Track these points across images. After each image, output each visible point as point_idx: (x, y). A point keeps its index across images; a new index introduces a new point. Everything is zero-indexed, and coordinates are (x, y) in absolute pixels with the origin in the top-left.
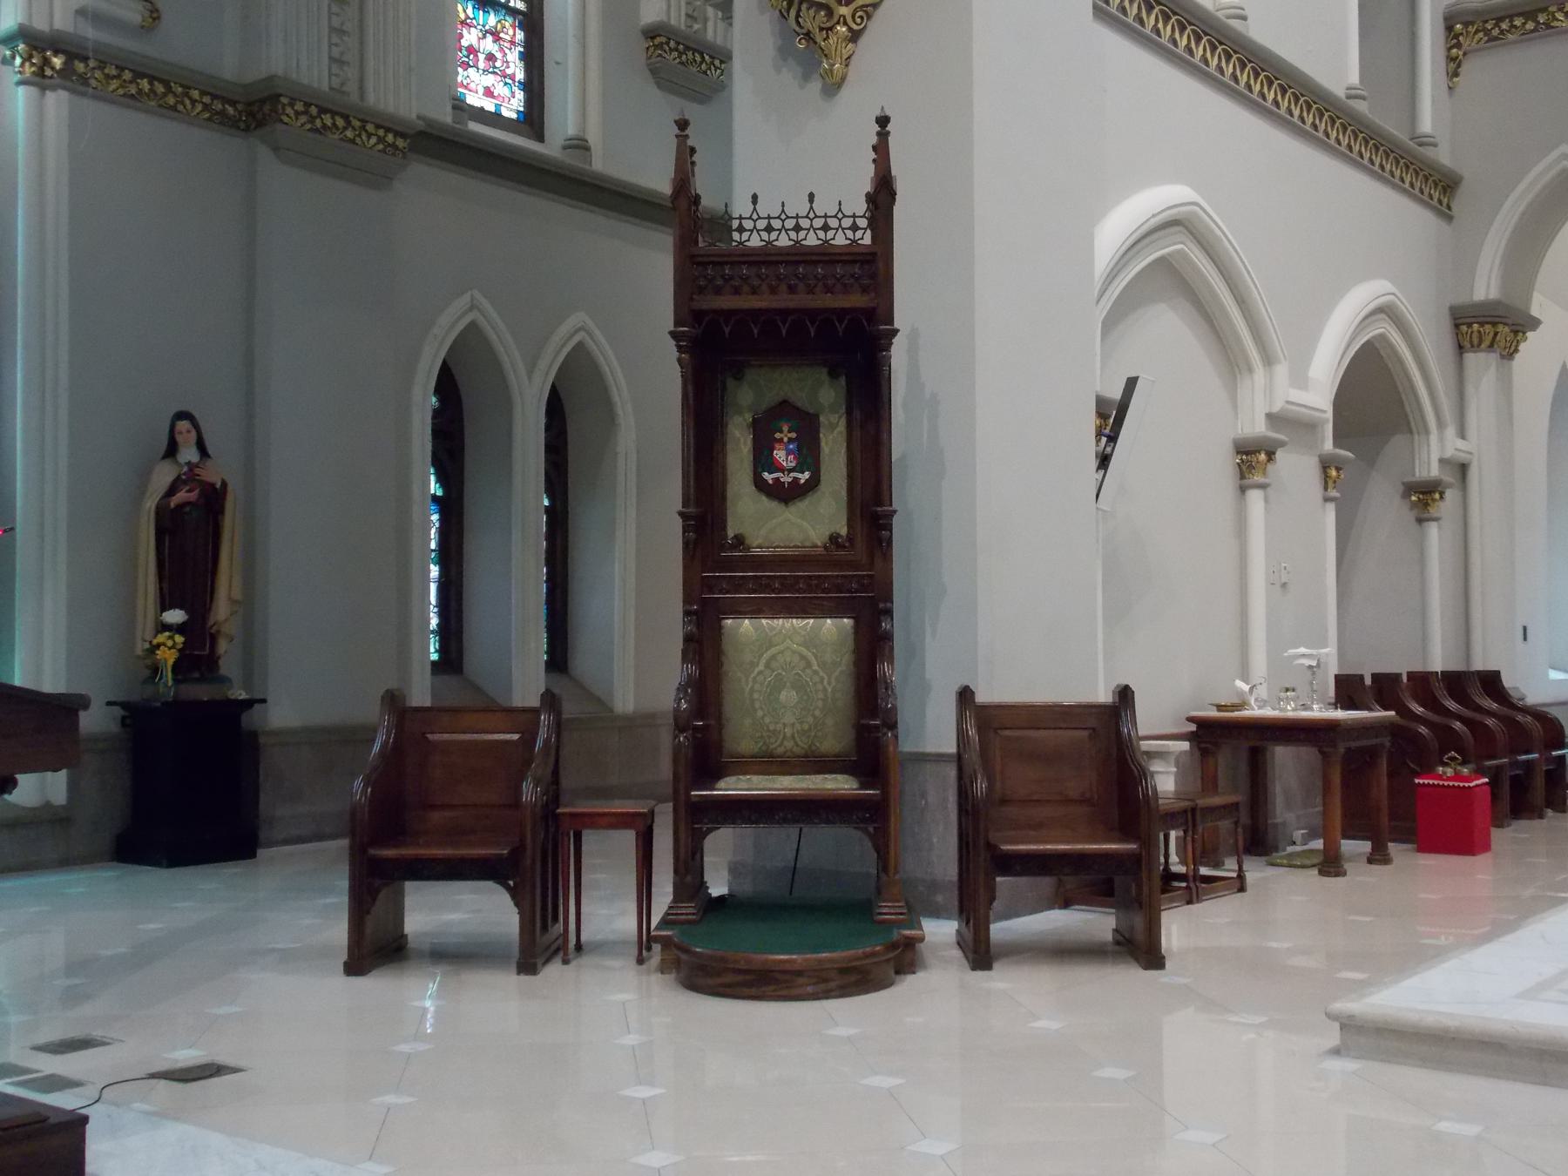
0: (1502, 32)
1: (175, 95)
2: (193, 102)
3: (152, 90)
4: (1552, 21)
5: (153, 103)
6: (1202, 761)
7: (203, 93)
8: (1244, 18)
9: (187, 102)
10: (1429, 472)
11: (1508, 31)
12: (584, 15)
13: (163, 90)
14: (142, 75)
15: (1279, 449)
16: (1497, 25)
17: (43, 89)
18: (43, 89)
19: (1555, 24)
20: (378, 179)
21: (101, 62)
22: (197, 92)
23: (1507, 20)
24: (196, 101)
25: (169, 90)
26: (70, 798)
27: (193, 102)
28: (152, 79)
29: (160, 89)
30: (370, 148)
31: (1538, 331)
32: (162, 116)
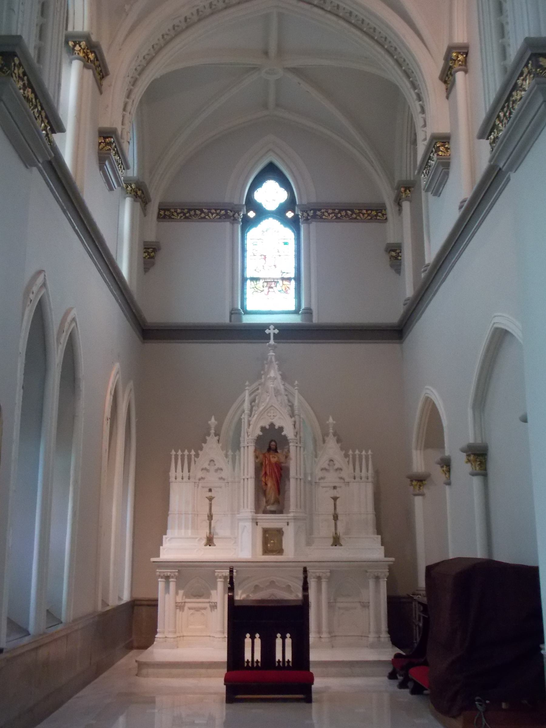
0: (190, 215)
1: (356, 214)
2: (363, 214)
5: (347, 219)
7: (367, 210)
9: (361, 215)
11: (193, 215)
14: (342, 210)
18: (309, 224)
19: (173, 217)
20: (28, 162)
21: (443, 142)
24: (365, 214)
25: (353, 212)
27: (363, 214)
28: (346, 210)
29: (349, 212)
30: (213, 218)
31: (279, 204)
32: (352, 222)
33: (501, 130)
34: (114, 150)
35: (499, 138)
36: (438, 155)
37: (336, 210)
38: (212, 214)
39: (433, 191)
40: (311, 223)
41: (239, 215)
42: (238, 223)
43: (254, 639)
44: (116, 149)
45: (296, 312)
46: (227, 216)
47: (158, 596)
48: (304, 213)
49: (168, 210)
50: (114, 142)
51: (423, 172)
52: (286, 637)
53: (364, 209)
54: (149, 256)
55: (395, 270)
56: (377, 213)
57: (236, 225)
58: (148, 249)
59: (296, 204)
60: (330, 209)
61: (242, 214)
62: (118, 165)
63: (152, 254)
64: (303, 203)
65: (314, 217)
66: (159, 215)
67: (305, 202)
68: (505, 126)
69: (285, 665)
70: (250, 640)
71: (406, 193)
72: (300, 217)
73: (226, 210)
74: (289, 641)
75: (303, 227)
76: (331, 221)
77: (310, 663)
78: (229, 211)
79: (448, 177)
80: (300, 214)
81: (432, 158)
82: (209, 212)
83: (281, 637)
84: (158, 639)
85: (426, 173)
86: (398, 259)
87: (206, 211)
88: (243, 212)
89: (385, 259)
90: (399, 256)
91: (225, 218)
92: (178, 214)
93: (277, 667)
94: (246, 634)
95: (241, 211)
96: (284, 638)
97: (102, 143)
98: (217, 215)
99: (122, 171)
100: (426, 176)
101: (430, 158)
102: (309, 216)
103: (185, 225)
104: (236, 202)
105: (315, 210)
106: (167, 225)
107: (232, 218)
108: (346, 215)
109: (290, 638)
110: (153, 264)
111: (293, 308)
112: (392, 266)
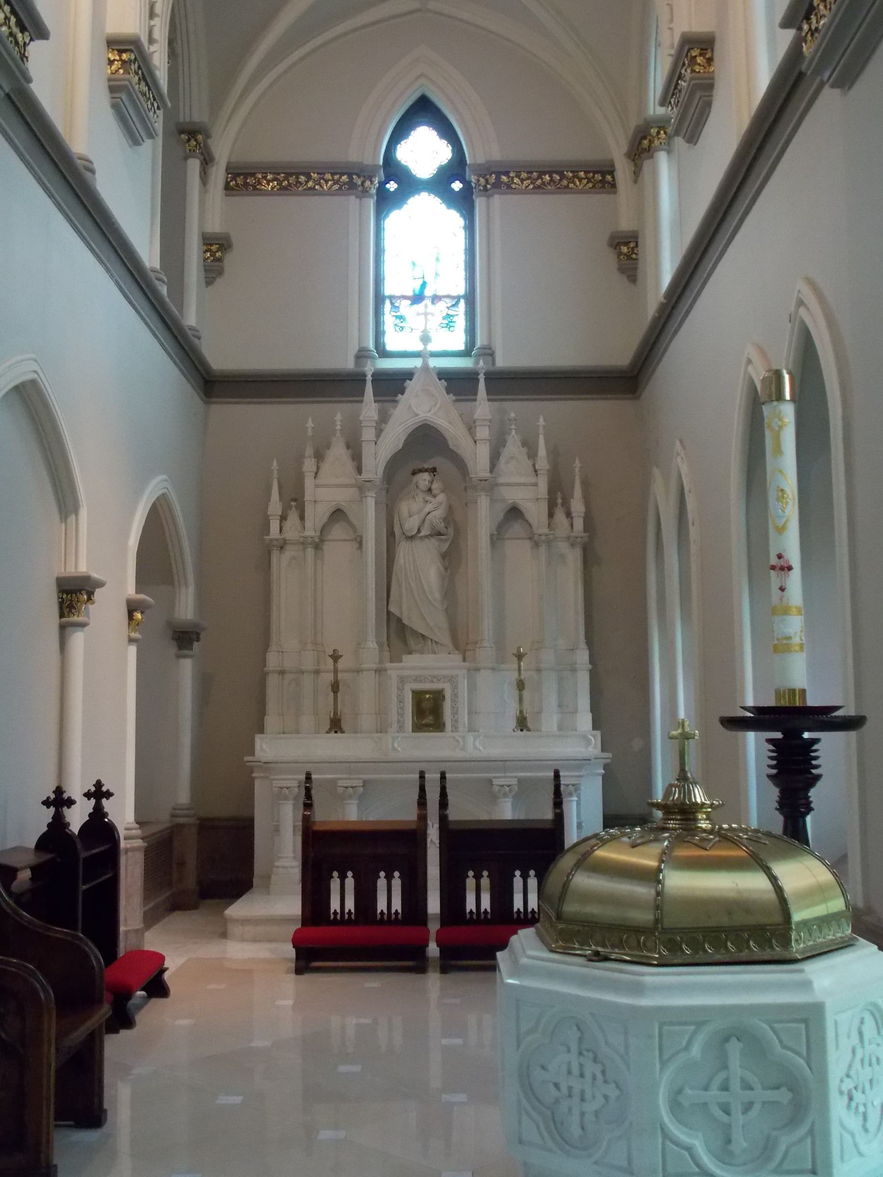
0: (290, 184)
3: (552, 180)
4: (258, 185)
6: (129, 623)
8: (199, 339)
10: (76, 567)
12: (175, 337)
13: (559, 178)
14: (545, 173)
15: (97, 590)
16: (286, 178)
17: (488, 197)
18: (488, 197)
22: (582, 173)
23: (294, 177)
25: (563, 176)
26: (254, 738)
27: (580, 180)
32: (561, 193)
33: (824, 16)
34: (137, 73)
35: (820, 30)
36: (693, 71)
37: (535, 173)
38: (327, 182)
39: (685, 134)
40: (492, 196)
41: (372, 182)
42: (371, 196)
43: (481, 878)
44: (140, 72)
45: (466, 353)
46: (351, 185)
47: (252, 807)
48: (481, 179)
49: (253, 175)
50: (135, 59)
51: (670, 103)
52: (379, 877)
53: (328, 173)
54: (212, 258)
55: (628, 278)
56: (604, 177)
57: (365, 200)
58: (211, 245)
59: (466, 163)
60: (524, 172)
61: (376, 182)
62: (146, 100)
63: (218, 254)
64: (478, 162)
65: (497, 185)
66: (227, 187)
67: (481, 159)
68: (830, 9)
69: (527, 916)
70: (338, 881)
71: (659, 136)
72: (473, 185)
73: (350, 176)
74: (397, 883)
75: (479, 203)
76: (526, 192)
77: (429, 917)
78: (354, 176)
79: (710, 112)
80: (473, 181)
81: (683, 75)
82: (574, 177)
83: (535, 876)
84: (280, 870)
85: (675, 103)
86: (632, 259)
87: (314, 176)
88: (380, 177)
89: (610, 260)
90: (633, 253)
91: (348, 189)
92: (522, 180)
93: (469, 920)
94: (515, 870)
95: (375, 176)
96: (343, 877)
97: (116, 62)
98: (334, 184)
99: (155, 112)
100: (675, 109)
101: (680, 77)
102: (489, 184)
103: (292, 202)
104: (368, 161)
105: (499, 174)
106: (247, 203)
107: (360, 189)
108: (296, 183)
109: (473, 877)
110: (220, 272)
111: (461, 346)
112: (622, 270)
